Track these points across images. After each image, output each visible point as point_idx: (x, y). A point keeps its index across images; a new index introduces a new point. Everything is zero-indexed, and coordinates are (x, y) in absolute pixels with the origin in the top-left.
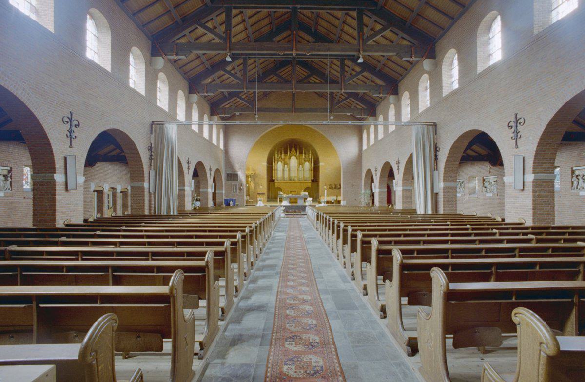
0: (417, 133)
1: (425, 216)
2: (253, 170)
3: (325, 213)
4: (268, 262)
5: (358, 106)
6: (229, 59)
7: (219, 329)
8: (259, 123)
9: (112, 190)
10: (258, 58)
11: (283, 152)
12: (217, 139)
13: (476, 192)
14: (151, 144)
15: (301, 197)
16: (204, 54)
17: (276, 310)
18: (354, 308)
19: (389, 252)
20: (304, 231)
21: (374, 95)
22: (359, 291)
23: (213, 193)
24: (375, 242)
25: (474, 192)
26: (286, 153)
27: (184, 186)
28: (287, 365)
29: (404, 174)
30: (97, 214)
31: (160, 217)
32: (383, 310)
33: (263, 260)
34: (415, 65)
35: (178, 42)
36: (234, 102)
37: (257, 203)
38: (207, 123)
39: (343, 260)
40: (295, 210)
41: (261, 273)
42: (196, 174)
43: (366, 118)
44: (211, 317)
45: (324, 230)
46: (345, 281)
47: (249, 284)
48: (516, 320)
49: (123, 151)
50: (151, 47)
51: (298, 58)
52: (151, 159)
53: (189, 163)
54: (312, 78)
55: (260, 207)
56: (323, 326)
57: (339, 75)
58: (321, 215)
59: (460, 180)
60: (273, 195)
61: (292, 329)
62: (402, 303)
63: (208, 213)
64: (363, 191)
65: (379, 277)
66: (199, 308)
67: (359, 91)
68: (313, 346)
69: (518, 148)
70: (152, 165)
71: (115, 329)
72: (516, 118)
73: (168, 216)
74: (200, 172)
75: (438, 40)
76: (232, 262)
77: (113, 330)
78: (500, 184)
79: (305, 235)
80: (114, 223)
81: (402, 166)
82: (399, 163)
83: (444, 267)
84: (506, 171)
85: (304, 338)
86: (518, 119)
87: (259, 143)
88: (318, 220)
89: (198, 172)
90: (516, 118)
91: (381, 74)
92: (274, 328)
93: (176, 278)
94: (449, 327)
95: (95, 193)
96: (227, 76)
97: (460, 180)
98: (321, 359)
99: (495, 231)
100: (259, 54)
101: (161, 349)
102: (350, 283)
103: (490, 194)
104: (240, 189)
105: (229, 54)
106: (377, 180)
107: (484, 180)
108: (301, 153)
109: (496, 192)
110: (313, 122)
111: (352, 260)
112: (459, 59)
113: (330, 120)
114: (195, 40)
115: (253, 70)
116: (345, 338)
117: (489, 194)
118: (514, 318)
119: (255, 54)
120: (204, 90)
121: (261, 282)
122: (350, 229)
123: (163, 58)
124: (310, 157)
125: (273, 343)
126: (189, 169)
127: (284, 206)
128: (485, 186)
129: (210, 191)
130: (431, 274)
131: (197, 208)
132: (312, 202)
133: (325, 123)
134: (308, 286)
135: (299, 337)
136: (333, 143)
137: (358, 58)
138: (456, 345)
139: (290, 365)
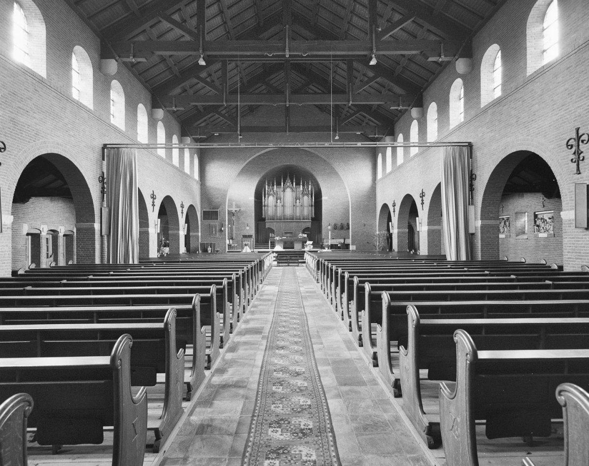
0: (446, 155)
1: (457, 263)
2: (237, 206)
3: (328, 260)
4: (251, 325)
5: (371, 123)
6: (202, 63)
7: (183, 412)
8: (243, 146)
9: (52, 233)
10: (240, 61)
11: (275, 184)
12: (190, 164)
13: (526, 232)
14: (103, 173)
15: (298, 240)
16: (171, 56)
17: (258, 386)
18: (362, 383)
19: (404, 309)
20: (301, 283)
21: (391, 108)
22: (368, 361)
23: (186, 236)
24: (385, 296)
25: (524, 233)
26: (279, 184)
27: (148, 227)
28: (269, 458)
29: (430, 210)
30: (32, 263)
31: (115, 267)
32: (397, 386)
33: (247, 322)
34: (444, 68)
35: (136, 39)
36: (211, 119)
37: (243, 248)
38: (178, 146)
39: (348, 320)
40: (292, 257)
41: (243, 339)
42: (162, 213)
43: (382, 138)
44: (172, 397)
45: (325, 282)
46: (350, 348)
47: (227, 352)
48: (561, 399)
49: (66, 183)
50: (99, 46)
51: (292, 60)
52: (103, 192)
53: (153, 197)
54: (311, 86)
55: (246, 254)
56: (319, 408)
57: (346, 82)
58: (322, 263)
59: (504, 217)
60: (263, 237)
61: (279, 410)
62: (421, 377)
63: (178, 262)
64: (378, 232)
65: (392, 342)
66: (157, 385)
67: (372, 103)
68: (304, 434)
69: (580, 173)
70: (105, 200)
71: (28, 414)
72: (578, 133)
73: (126, 265)
74: (168, 210)
75: (476, 32)
76: (203, 324)
77: (25, 416)
78: (556, 219)
79: (301, 289)
80: (53, 275)
81: (428, 200)
82: (423, 196)
83: (468, 328)
84: (563, 204)
85: (293, 422)
86: (580, 135)
87: (246, 171)
88: (318, 269)
89: (167, 208)
90: (578, 133)
91: (399, 81)
92: (255, 410)
93: (121, 345)
94: (476, 410)
95: (30, 237)
96: (201, 84)
97: (504, 217)
98: (314, 451)
99: (548, 282)
100: (242, 56)
101: (100, 439)
102: (356, 350)
103: (545, 235)
104: (221, 231)
105: (202, 56)
106: (395, 219)
107: (536, 216)
108: (298, 184)
109: (552, 232)
110: (313, 144)
111: (359, 320)
112: (503, 57)
113: (334, 142)
114: (158, 38)
115: (235, 77)
116: (348, 423)
117: (543, 235)
118: (559, 397)
119: (236, 56)
120: (171, 103)
121: (241, 352)
122: (356, 280)
123: (116, 61)
124: (310, 189)
125: (253, 430)
126: (153, 205)
127: (276, 252)
128: (537, 223)
129: (182, 233)
130: (454, 338)
131: (165, 255)
132: (312, 246)
133: (327, 145)
134: (302, 354)
135: (286, 422)
136: (341, 174)
137: (371, 59)
138: (490, 434)
139: (272, 459)
